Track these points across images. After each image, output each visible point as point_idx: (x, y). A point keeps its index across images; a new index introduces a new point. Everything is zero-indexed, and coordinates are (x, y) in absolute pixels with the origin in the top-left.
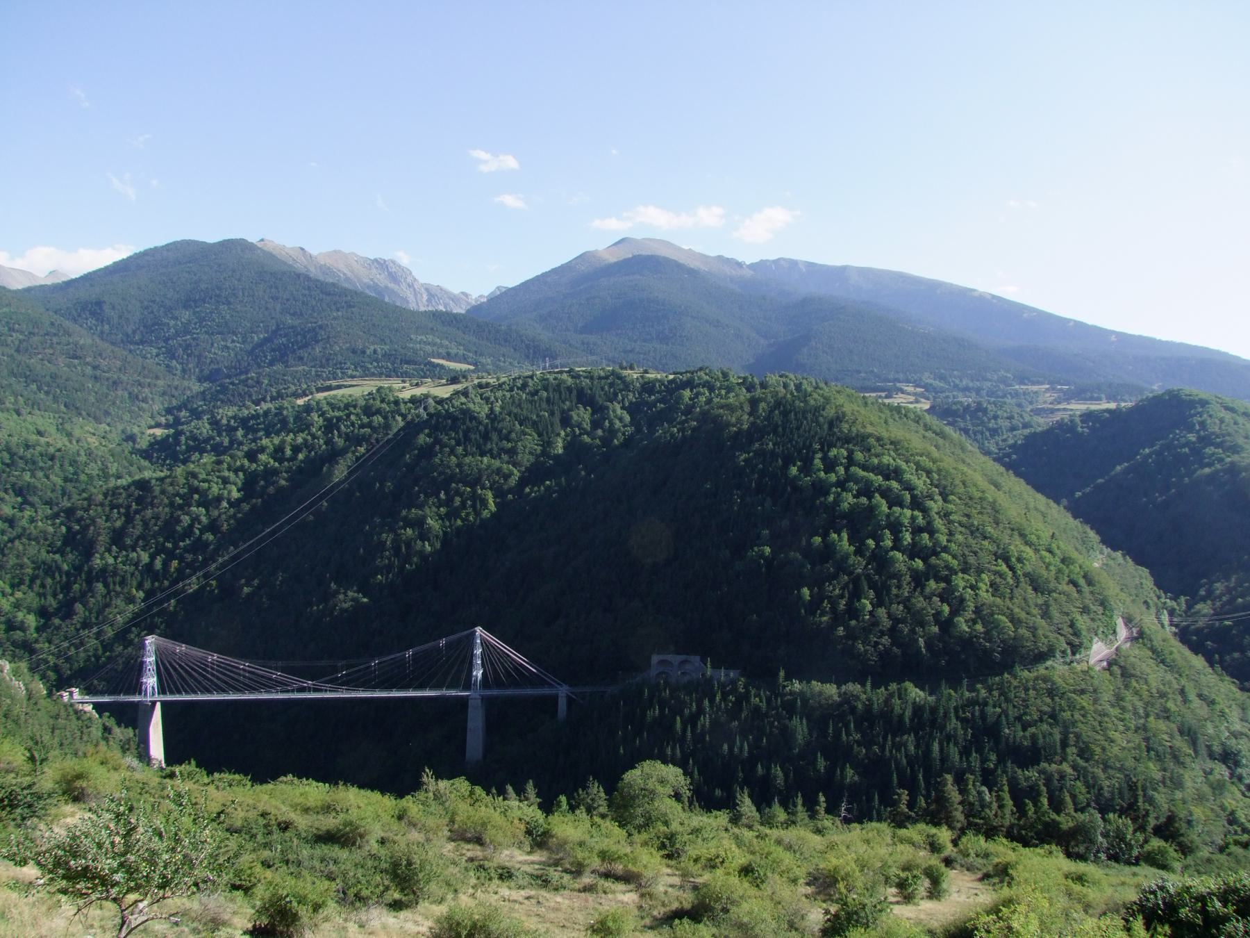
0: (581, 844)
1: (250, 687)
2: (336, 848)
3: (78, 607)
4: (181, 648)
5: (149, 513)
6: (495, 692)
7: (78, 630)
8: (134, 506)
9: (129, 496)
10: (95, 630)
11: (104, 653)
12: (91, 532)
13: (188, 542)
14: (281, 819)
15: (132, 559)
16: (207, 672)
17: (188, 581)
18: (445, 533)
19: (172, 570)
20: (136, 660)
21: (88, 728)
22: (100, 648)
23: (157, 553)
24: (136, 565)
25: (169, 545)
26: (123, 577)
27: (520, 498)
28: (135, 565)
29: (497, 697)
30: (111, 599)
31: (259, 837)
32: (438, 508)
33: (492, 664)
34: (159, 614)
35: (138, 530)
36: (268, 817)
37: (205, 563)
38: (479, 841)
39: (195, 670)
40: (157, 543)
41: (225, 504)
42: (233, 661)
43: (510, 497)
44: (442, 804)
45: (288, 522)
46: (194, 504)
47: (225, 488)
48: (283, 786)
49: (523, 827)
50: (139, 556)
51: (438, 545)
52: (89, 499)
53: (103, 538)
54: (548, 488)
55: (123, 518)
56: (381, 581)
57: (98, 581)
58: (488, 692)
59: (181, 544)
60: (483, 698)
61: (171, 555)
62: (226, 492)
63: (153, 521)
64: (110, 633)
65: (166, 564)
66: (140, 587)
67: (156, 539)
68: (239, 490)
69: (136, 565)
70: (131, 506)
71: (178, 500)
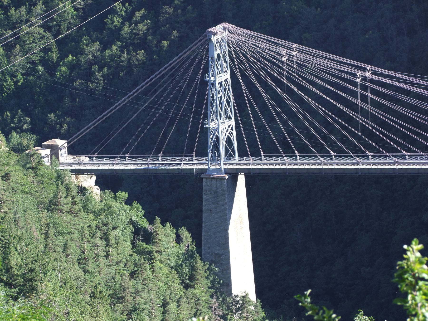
1: (414, 142)
22: (54, 48)
39: (301, 102)
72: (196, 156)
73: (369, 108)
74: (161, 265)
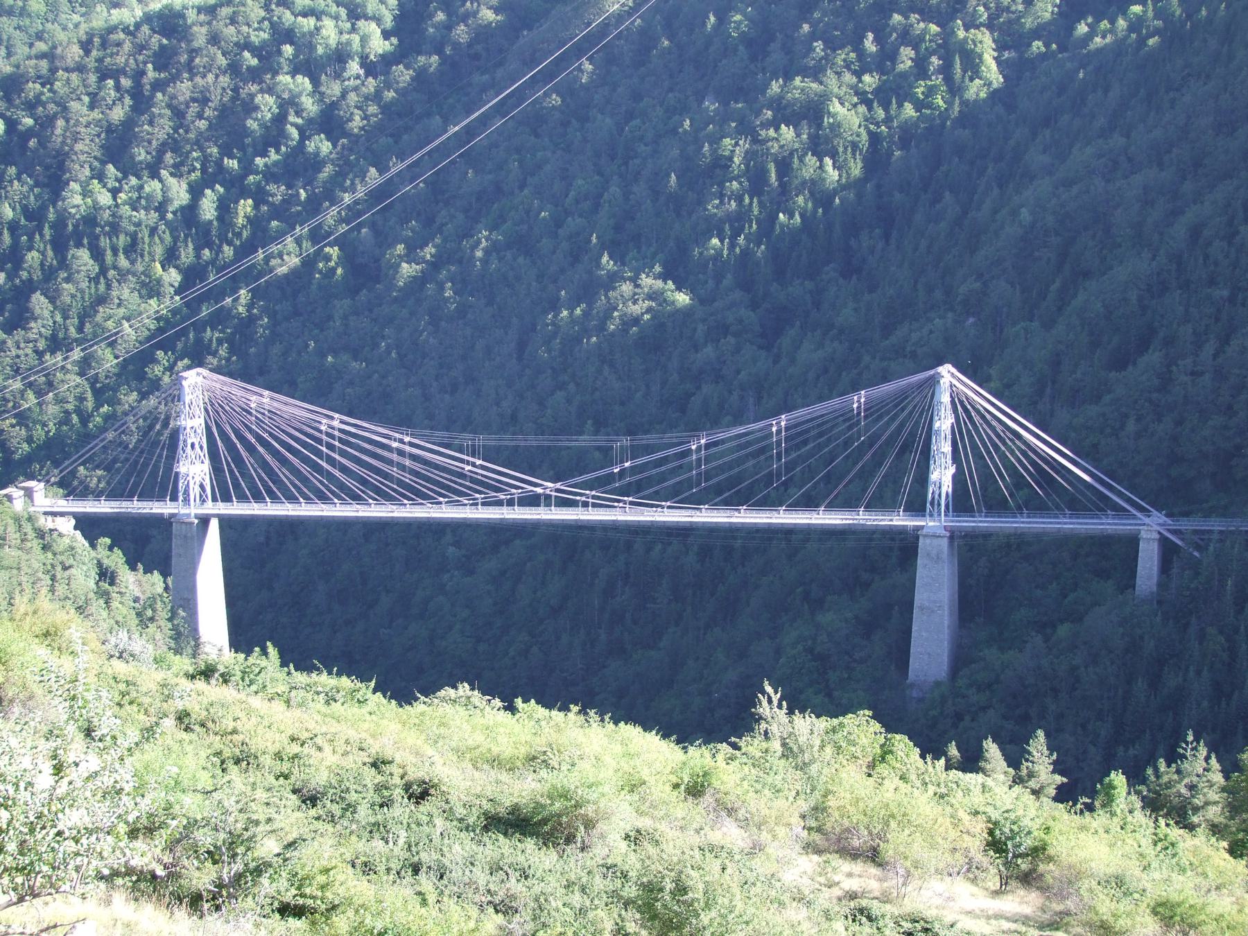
0: (1119, 882)
2: (530, 843)
3: (39, 302)
4: (262, 400)
5: (184, 89)
6: (980, 522)
7: (40, 354)
8: (151, 74)
9: (141, 48)
10: (77, 354)
11: (97, 408)
12: (58, 131)
13: (274, 156)
14: (414, 774)
15: (149, 198)
16: (319, 453)
17: (274, 248)
18: (874, 138)
19: (240, 221)
20: (166, 424)
21: (65, 568)
22: (89, 395)
23: (207, 181)
24: (161, 208)
25: (233, 164)
26: (134, 238)
27: (1062, 48)
28: (157, 209)
29: (987, 535)
30: (109, 287)
31: (363, 813)
32: (858, 74)
33: (978, 456)
34: (219, 319)
35: (163, 128)
36: (387, 769)
37: (314, 206)
38: (873, 856)
40: (205, 160)
41: (354, 67)
42: (375, 431)
43: (1037, 46)
44: (803, 767)
45: (500, 109)
46: (286, 69)
47: (354, 29)
48: (448, 708)
49: (980, 827)
50: (165, 190)
51: (856, 169)
52: (50, 56)
53: (86, 148)
54: (1136, 25)
55: (128, 101)
56: (719, 253)
57: (79, 245)
58: (967, 523)
59: (259, 161)
60: (953, 535)
61: (236, 187)
62: (356, 39)
63: (194, 108)
64: (108, 361)
65: (225, 208)
66: (170, 258)
67: (202, 149)
68: (386, 35)
69: (161, 208)
70: (143, 73)
71: (250, 60)
72: (170, 500)
73: (407, 462)
74: (120, 606)
